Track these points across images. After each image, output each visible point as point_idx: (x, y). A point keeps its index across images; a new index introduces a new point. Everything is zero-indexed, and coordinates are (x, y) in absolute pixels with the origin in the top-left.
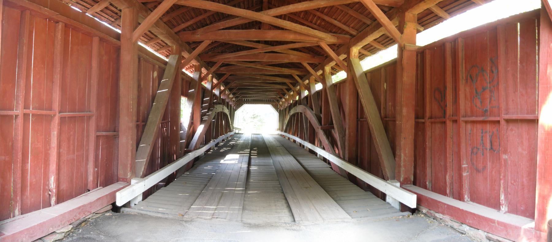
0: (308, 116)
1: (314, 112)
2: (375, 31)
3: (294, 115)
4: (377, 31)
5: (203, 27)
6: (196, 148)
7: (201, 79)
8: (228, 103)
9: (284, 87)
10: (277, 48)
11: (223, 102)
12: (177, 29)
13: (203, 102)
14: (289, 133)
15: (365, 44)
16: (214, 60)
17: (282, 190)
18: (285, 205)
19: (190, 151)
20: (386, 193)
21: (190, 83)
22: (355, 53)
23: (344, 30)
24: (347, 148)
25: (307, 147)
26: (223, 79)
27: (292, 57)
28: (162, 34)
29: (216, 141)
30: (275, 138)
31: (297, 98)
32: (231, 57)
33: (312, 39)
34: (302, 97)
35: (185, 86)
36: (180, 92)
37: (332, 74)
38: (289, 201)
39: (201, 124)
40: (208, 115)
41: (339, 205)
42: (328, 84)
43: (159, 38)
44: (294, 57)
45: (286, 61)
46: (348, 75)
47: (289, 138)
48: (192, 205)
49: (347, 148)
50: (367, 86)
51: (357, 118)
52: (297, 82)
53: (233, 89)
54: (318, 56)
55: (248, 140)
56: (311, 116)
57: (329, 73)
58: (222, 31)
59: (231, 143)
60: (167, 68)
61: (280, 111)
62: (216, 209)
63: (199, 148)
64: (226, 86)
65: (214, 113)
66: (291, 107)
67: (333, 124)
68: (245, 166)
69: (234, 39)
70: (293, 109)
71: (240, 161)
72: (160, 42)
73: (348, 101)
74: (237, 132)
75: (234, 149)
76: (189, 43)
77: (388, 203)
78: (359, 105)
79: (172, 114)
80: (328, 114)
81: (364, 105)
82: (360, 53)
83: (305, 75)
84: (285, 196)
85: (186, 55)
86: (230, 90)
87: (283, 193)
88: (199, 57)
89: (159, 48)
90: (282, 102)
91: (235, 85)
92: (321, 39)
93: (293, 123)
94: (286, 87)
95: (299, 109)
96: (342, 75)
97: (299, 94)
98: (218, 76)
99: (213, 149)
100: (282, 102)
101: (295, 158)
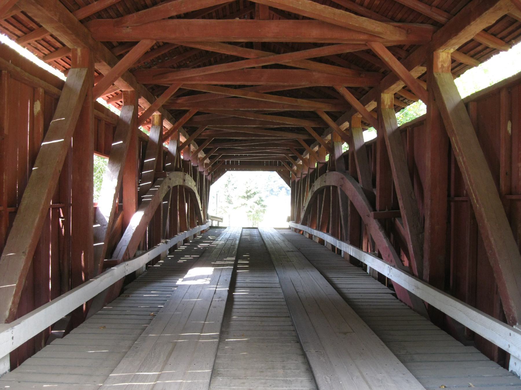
0: (348, 194)
1: (360, 185)
2: (487, 9)
3: (320, 191)
4: (491, 10)
5: (138, 10)
6: (128, 257)
7: (137, 120)
8: (195, 169)
9: (301, 137)
10: (286, 59)
11: (185, 167)
12: (83, 14)
13: (143, 167)
14: (311, 226)
15: (464, 41)
16: (163, 81)
17: (297, 336)
18: (303, 368)
19: (115, 264)
20: (512, 351)
21: (115, 128)
22: (443, 62)
23: (419, 14)
24: (426, 256)
25: (345, 253)
26: (183, 120)
27: (316, 75)
28: (51, 21)
29: (172, 242)
30: (283, 235)
31: (327, 158)
32: (196, 77)
33: (356, 36)
34: (337, 155)
35: (105, 135)
36: (92, 145)
37: (398, 109)
38: (310, 358)
39: (138, 208)
40: (154, 192)
41: (411, 371)
42: (389, 129)
43: (46, 31)
44: (321, 76)
45: (305, 84)
46: (428, 109)
47: (311, 236)
48: (112, 372)
49: (426, 256)
50: (470, 130)
51: (449, 195)
52: (327, 126)
53: (204, 140)
54: (368, 73)
55: (234, 239)
56: (354, 193)
57: (390, 107)
58: (176, 21)
59: (201, 245)
60: (64, 94)
61: (294, 182)
62: (158, 377)
63: (135, 257)
64: (190, 135)
65: (166, 187)
66: (314, 176)
67: (398, 208)
68: (224, 290)
69: (199, 40)
70: (319, 179)
71: (215, 281)
72: (49, 38)
73: (428, 161)
74: (215, 224)
75: (204, 257)
76: (110, 45)
77: (514, 374)
78: (453, 170)
79: (75, 188)
80: (389, 189)
81: (463, 169)
82: (453, 61)
83: (343, 112)
84: (302, 349)
85: (103, 68)
86: (200, 143)
87: (298, 342)
88: (132, 75)
89: (46, 52)
90: (298, 166)
91: (208, 132)
92: (373, 35)
93: (315, 205)
94: (306, 137)
95: (331, 179)
96: (417, 109)
97: (331, 150)
98: (173, 114)
99: (166, 258)
100: (298, 166)
101: (322, 273)
